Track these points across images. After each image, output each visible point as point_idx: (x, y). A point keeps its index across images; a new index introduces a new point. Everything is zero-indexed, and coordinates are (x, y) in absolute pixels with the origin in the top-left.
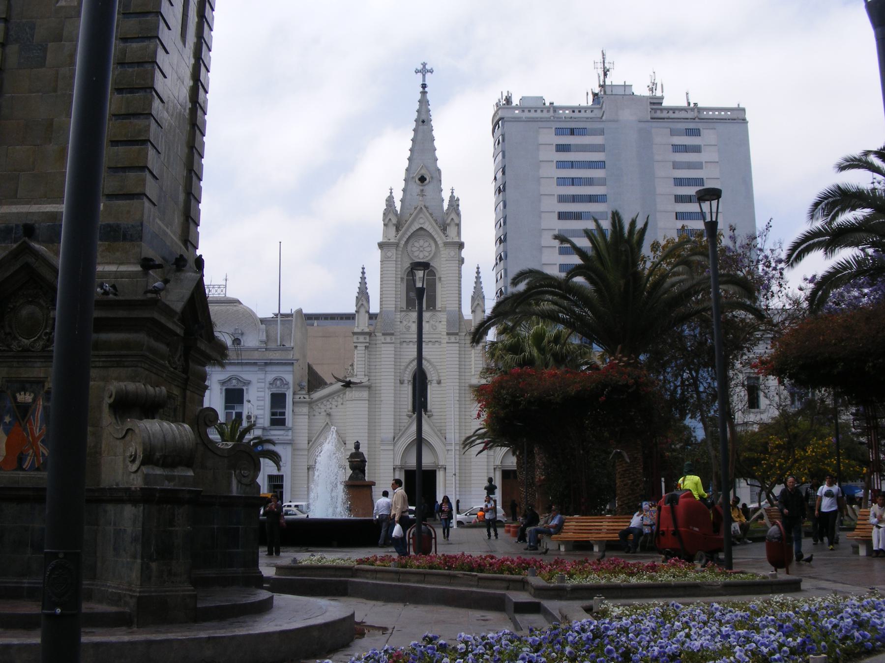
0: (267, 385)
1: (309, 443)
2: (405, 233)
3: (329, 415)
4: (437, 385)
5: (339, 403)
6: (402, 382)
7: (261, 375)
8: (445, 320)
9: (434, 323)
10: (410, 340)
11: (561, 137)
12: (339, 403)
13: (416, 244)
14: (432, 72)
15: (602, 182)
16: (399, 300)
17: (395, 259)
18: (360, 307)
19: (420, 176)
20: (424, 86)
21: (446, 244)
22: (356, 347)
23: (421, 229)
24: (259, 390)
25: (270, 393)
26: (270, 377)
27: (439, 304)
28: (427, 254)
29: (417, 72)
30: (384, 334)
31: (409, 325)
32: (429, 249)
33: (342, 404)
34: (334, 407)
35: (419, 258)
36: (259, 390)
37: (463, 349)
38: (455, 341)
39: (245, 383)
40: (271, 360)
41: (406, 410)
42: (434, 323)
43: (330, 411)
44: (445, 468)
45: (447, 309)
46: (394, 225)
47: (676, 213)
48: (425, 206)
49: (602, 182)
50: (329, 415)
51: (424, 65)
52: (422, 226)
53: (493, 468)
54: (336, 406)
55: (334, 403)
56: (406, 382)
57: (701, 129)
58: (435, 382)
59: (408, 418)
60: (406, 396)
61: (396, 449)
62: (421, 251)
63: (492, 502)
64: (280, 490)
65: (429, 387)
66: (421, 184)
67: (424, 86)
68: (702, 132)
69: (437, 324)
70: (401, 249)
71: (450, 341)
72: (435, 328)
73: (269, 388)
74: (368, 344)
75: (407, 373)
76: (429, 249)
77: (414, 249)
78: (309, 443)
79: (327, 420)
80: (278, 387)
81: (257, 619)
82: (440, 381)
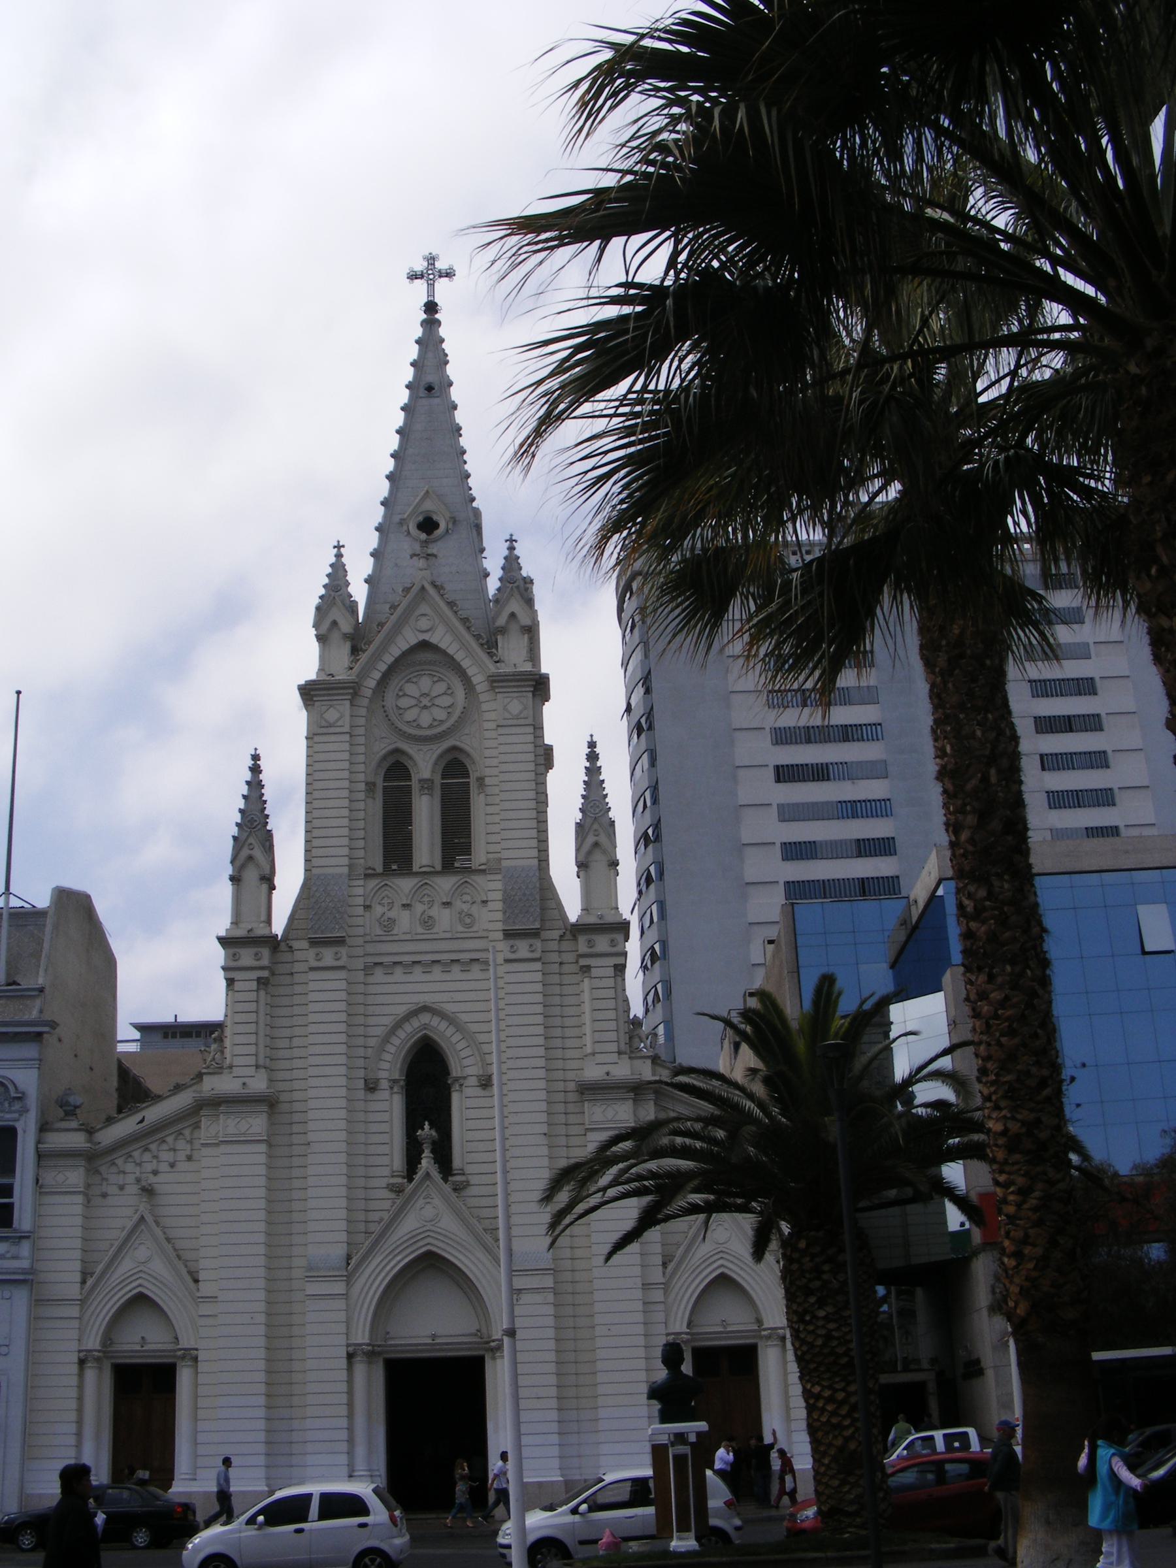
1: (84, 1282)
2: (377, 657)
4: (479, 1092)
6: (371, 1087)
8: (498, 895)
9: (465, 907)
10: (454, 956)
12: (181, 1156)
13: (411, 689)
14: (433, 259)
16: (361, 843)
17: (347, 729)
18: (589, 853)
19: (421, 518)
20: (431, 307)
22: (586, 969)
23: (424, 645)
28: (440, 714)
29: (414, 276)
32: (445, 701)
34: (164, 1167)
35: (419, 727)
37: (556, 979)
38: (530, 955)
41: (386, 1172)
42: (465, 907)
43: (152, 1179)
45: (505, 863)
47: (1042, 756)
48: (433, 584)
51: (431, 260)
52: (426, 637)
54: (172, 1165)
56: (384, 1084)
58: (473, 1081)
59: (393, 1196)
62: (425, 707)
65: (455, 1097)
67: (431, 307)
70: (365, 702)
71: (320, 964)
72: (468, 921)
74: (265, 974)
75: (392, 1049)
76: (445, 701)
77: (404, 702)
78: (84, 1282)
79: (143, 1208)
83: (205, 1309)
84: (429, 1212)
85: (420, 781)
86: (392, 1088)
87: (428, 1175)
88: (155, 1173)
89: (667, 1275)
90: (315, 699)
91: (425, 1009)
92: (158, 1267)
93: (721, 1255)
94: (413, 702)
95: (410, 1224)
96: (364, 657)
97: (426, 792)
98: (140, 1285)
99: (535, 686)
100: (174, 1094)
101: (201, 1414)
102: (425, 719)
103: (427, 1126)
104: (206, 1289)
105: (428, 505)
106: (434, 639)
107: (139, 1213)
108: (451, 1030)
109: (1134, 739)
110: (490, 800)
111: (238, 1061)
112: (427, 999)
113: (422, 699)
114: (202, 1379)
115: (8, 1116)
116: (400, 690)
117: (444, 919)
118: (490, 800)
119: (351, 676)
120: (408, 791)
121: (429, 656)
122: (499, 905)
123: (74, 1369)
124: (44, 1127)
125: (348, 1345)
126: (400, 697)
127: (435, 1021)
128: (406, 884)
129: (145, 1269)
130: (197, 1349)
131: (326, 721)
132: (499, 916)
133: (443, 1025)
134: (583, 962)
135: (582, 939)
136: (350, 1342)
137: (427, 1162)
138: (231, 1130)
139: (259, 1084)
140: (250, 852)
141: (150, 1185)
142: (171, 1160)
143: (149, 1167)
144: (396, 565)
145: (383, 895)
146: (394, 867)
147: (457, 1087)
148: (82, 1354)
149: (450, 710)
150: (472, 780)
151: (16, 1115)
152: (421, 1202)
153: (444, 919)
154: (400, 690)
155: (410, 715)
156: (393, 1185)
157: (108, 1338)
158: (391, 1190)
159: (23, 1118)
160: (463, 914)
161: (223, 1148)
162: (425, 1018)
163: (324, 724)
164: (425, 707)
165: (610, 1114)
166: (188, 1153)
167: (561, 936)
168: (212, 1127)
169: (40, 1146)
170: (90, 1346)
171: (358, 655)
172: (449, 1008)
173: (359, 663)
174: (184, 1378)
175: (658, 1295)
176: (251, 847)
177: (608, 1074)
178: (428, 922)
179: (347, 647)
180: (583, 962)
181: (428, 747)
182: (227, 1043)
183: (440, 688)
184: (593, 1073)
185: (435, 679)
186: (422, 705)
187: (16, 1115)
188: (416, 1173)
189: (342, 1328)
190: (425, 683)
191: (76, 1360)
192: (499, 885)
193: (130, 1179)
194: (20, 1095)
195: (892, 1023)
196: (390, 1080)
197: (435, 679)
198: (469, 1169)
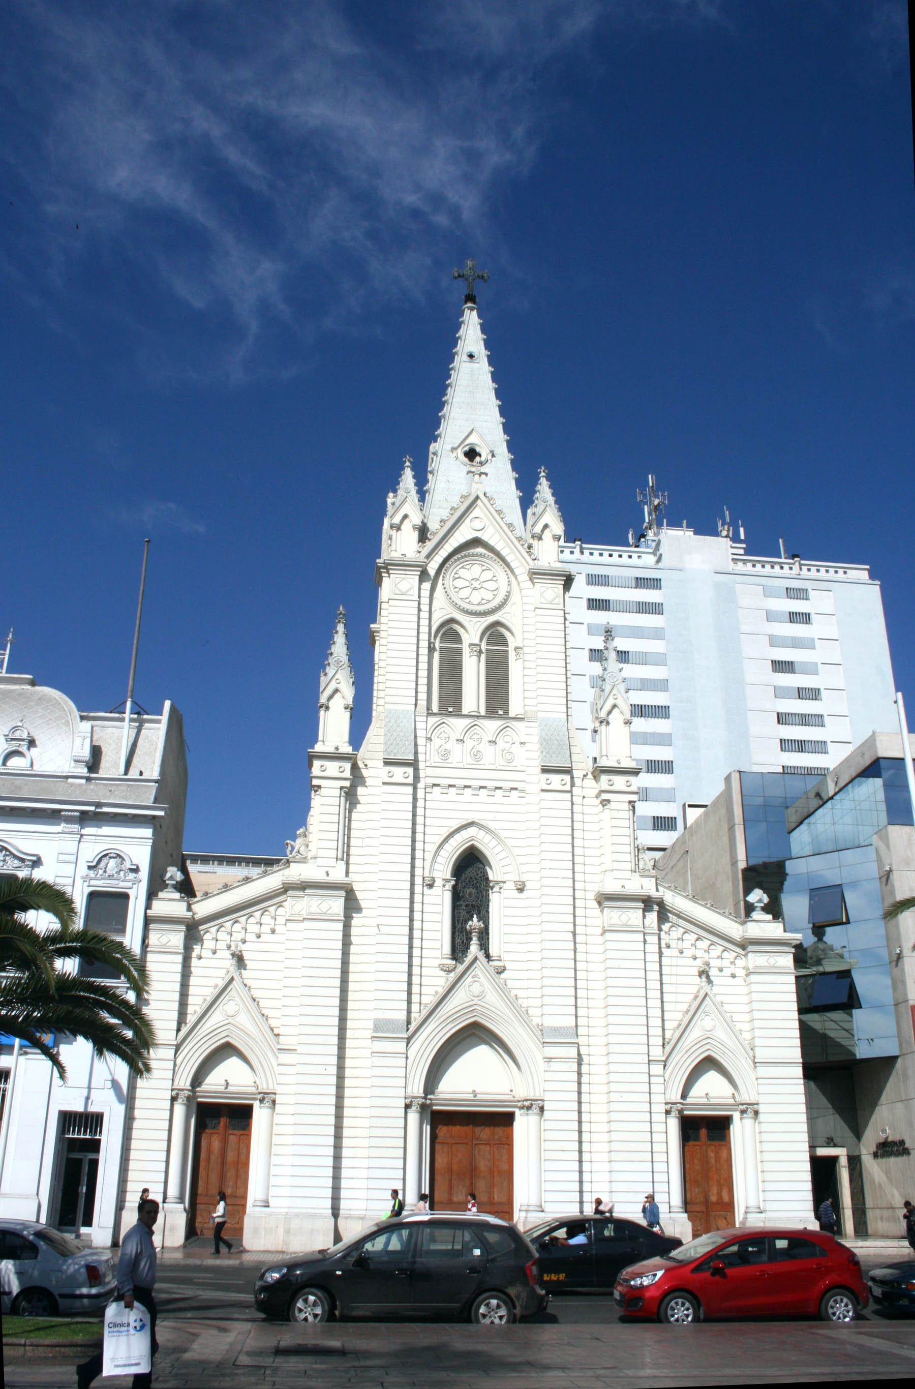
0: (83, 870)
1: (178, 1030)
3: (240, 960)
5: (266, 929)
7: (70, 845)
8: (536, 739)
9: (507, 746)
11: (604, 573)
12: (266, 929)
13: (462, 573)
15: (659, 660)
19: (467, 448)
21: (535, 575)
23: (476, 542)
24: (62, 858)
25: (87, 890)
26: (90, 850)
27: (515, 708)
28: (489, 596)
30: (388, 763)
31: (448, 746)
32: (491, 585)
33: (273, 931)
34: (250, 937)
36: (62, 858)
39: (23, 860)
40: (99, 805)
41: (438, 954)
42: (507, 746)
43: (242, 947)
44: (542, 1109)
45: (540, 715)
46: (414, 527)
47: (778, 714)
49: (659, 660)
50: (240, 960)
53: (663, 1108)
54: (259, 936)
55: (253, 928)
56: (439, 883)
57: (810, 590)
58: (511, 885)
59: (443, 974)
60: (438, 917)
61: (412, 1052)
62: (475, 589)
63: (206, 1228)
64: (92, 1156)
66: (469, 463)
68: (812, 594)
69: (516, 749)
73: (86, 878)
76: (491, 585)
77: (459, 583)
78: (178, 1030)
79: (233, 971)
80: (110, 877)
81: (6, 1279)
82: (524, 883)
83: (284, 1058)
84: (476, 989)
85: (471, 645)
86: (444, 886)
87: (476, 959)
88: (244, 942)
89: (667, 1054)
90: (391, 572)
91: (472, 824)
92: (244, 1020)
93: (709, 1040)
94: (467, 584)
95: (459, 998)
96: (429, 545)
97: (475, 653)
98: (227, 1036)
99: (565, 581)
100: (263, 877)
101: (275, 1150)
102: (476, 597)
103: (475, 918)
104: (284, 1041)
105: (472, 440)
106: (485, 537)
107: (230, 974)
108: (494, 842)
109: (842, 708)
110: (527, 664)
111: (321, 853)
112: (470, 817)
113: (472, 582)
114: (277, 1119)
115: (122, 884)
116: (456, 573)
117: (490, 755)
118: (527, 664)
119: (422, 558)
120: (460, 652)
121: (480, 550)
122: (536, 747)
123: (402, 1112)
124: (151, 895)
125: (172, 1090)
126: (456, 578)
127: (481, 834)
128: (459, 724)
129: (233, 1022)
130: (275, 1094)
131: (400, 590)
132: (536, 755)
133: (488, 837)
134: (605, 796)
135: (604, 778)
136: (174, 1087)
137: (474, 948)
138: (314, 909)
139: (337, 875)
140: (338, 685)
141: (241, 951)
142: (258, 932)
143: (238, 936)
144: (448, 481)
145: (441, 730)
146: (450, 709)
147: (496, 889)
148: (408, 1101)
149: (495, 593)
150: (511, 649)
151: (130, 884)
152: (470, 979)
153: (490, 755)
154: (456, 573)
155: (464, 593)
156: (444, 965)
157: (197, 1080)
158: (442, 970)
159: (135, 887)
160: (506, 751)
161: (307, 924)
162: (472, 831)
163: (397, 592)
164: (475, 589)
165: (624, 918)
166: (273, 926)
167: (585, 776)
168: (295, 905)
169: (148, 911)
170: (181, 1086)
171: (425, 543)
172: (492, 825)
173: (425, 548)
174: (260, 1115)
175: (657, 1069)
176: (338, 681)
177: (623, 887)
178: (477, 755)
179: (415, 535)
180: (605, 796)
181: (478, 619)
182: (311, 837)
183: (488, 575)
184: (613, 887)
185: (484, 568)
186: (473, 586)
187: (130, 884)
188: (466, 956)
189: (402, 1082)
190: (476, 570)
191: (403, 1106)
192: (536, 731)
193: (222, 945)
194: (135, 867)
195: (787, 874)
196: (443, 879)
197: (484, 568)
198: (505, 957)
